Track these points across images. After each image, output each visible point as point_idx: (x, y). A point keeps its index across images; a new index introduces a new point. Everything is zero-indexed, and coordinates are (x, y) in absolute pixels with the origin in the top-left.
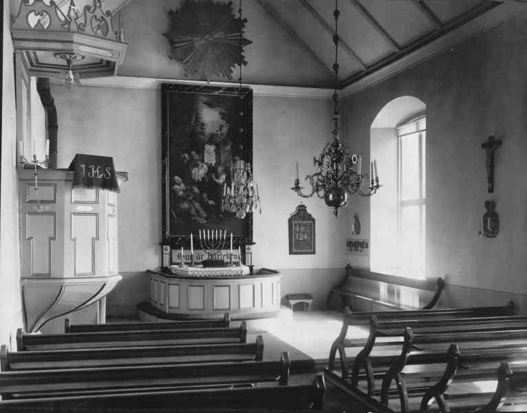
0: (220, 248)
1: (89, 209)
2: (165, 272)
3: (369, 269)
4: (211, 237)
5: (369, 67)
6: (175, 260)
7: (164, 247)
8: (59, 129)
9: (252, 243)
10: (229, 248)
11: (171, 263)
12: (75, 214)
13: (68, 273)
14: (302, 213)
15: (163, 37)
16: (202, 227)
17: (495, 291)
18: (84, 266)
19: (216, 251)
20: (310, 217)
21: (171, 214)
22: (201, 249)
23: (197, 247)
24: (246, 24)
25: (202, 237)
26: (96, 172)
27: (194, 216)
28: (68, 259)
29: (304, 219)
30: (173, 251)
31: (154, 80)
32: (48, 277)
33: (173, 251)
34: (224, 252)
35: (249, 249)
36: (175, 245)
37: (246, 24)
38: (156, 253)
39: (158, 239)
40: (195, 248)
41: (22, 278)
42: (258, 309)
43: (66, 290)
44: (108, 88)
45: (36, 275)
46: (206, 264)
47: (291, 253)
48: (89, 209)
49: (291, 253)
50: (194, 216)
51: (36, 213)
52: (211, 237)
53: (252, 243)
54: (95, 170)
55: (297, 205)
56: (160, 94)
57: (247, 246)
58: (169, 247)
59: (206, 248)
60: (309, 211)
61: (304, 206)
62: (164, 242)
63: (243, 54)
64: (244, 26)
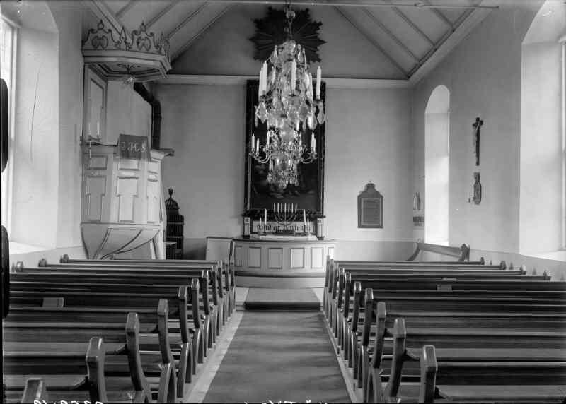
0: (291, 221)
1: (132, 174)
2: (246, 238)
3: (423, 241)
4: (280, 210)
5: (421, 60)
6: (255, 229)
7: (246, 218)
8: (162, 119)
9: (323, 217)
10: (303, 221)
11: (252, 232)
12: (121, 177)
13: (113, 218)
14: (370, 192)
15: (250, 42)
16: (277, 201)
17: (503, 253)
18: (126, 216)
19: (288, 223)
20: (377, 194)
21: (252, 189)
22: (275, 221)
23: (271, 218)
24: (320, 27)
25: (276, 210)
26: (133, 147)
27: (272, 192)
28: (109, 213)
29: (373, 196)
30: (253, 222)
31: (238, 78)
32: (98, 222)
33: (253, 222)
34: (298, 224)
35: (320, 222)
36: (254, 215)
37: (320, 27)
38: (239, 223)
39: (241, 211)
40: (269, 219)
41: (82, 223)
42: (307, 270)
43: (113, 232)
44: (348, 89)
45: (92, 221)
46: (277, 233)
47: (360, 226)
48: (132, 174)
49: (360, 226)
50: (272, 192)
51: (93, 177)
52: (280, 210)
53: (323, 217)
54: (134, 149)
55: (366, 184)
56: (245, 89)
57: (319, 219)
58: (249, 218)
59: (279, 220)
60: (377, 188)
61: (372, 184)
62: (246, 214)
63: (317, 52)
64: (319, 29)
